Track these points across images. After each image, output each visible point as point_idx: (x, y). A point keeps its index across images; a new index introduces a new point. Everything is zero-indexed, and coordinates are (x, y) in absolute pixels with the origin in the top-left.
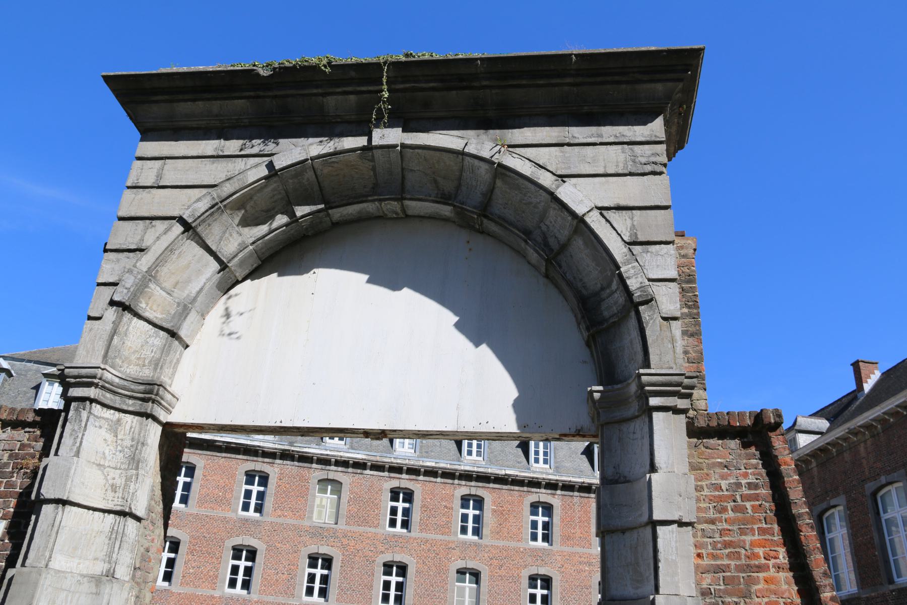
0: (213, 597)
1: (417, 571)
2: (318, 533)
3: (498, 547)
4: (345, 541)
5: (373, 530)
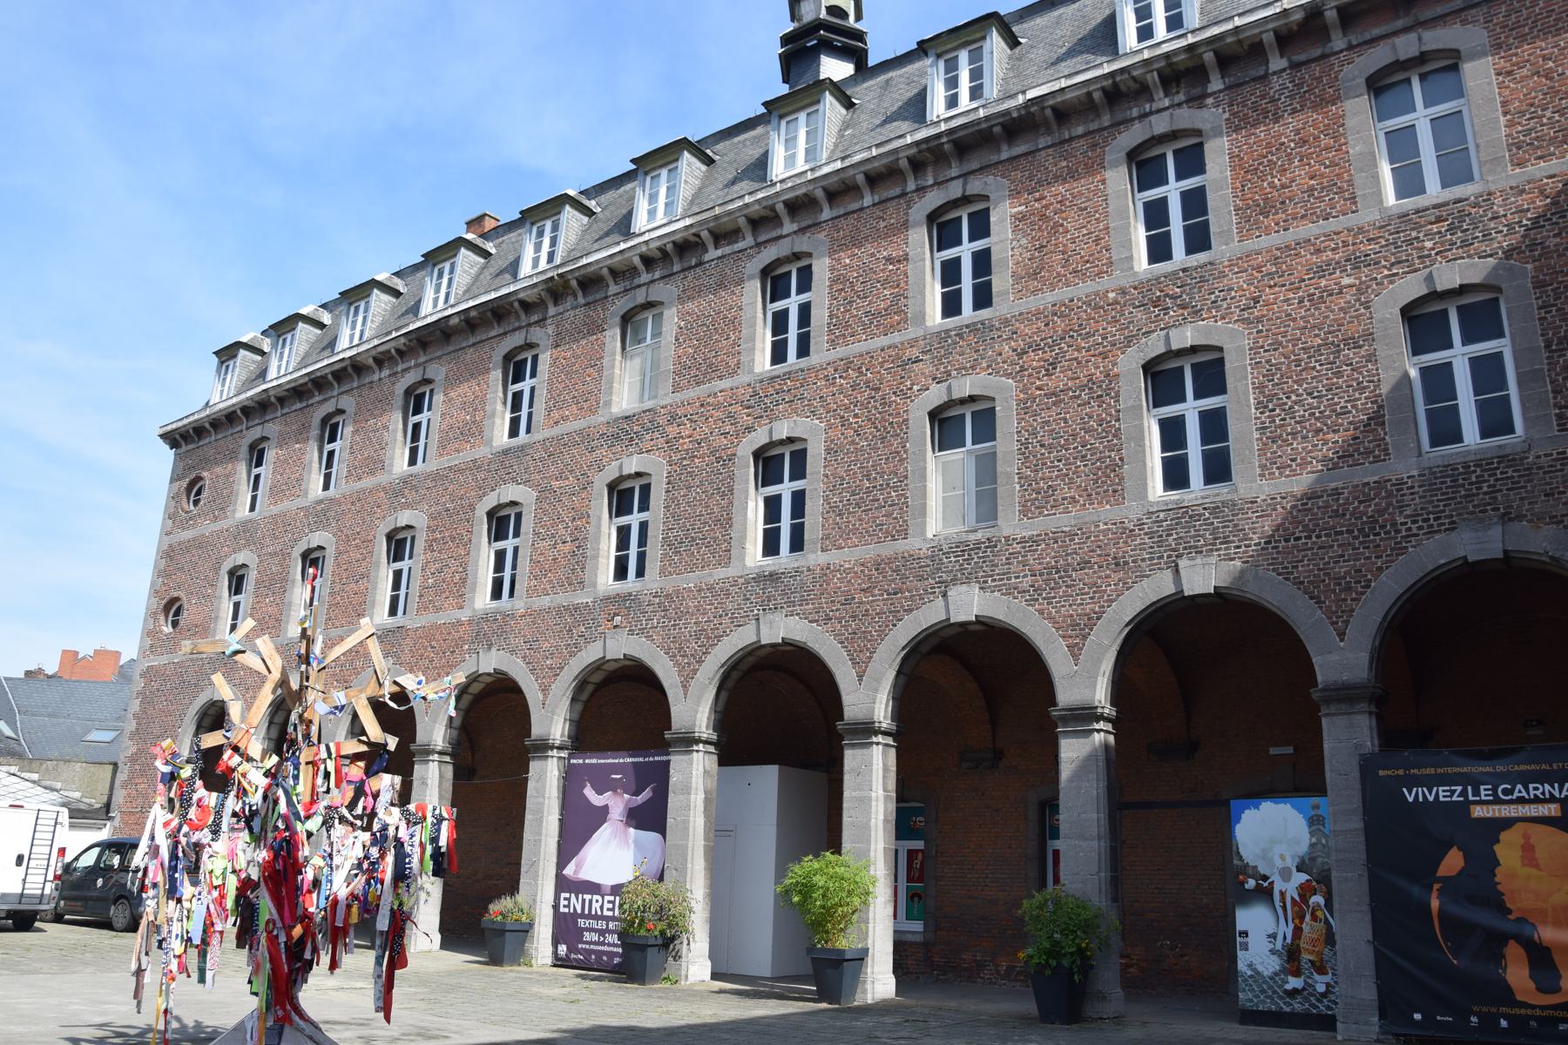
0: (460, 623)
1: (828, 451)
2: (627, 431)
3: (1038, 314)
4: (672, 431)
5: (726, 384)
